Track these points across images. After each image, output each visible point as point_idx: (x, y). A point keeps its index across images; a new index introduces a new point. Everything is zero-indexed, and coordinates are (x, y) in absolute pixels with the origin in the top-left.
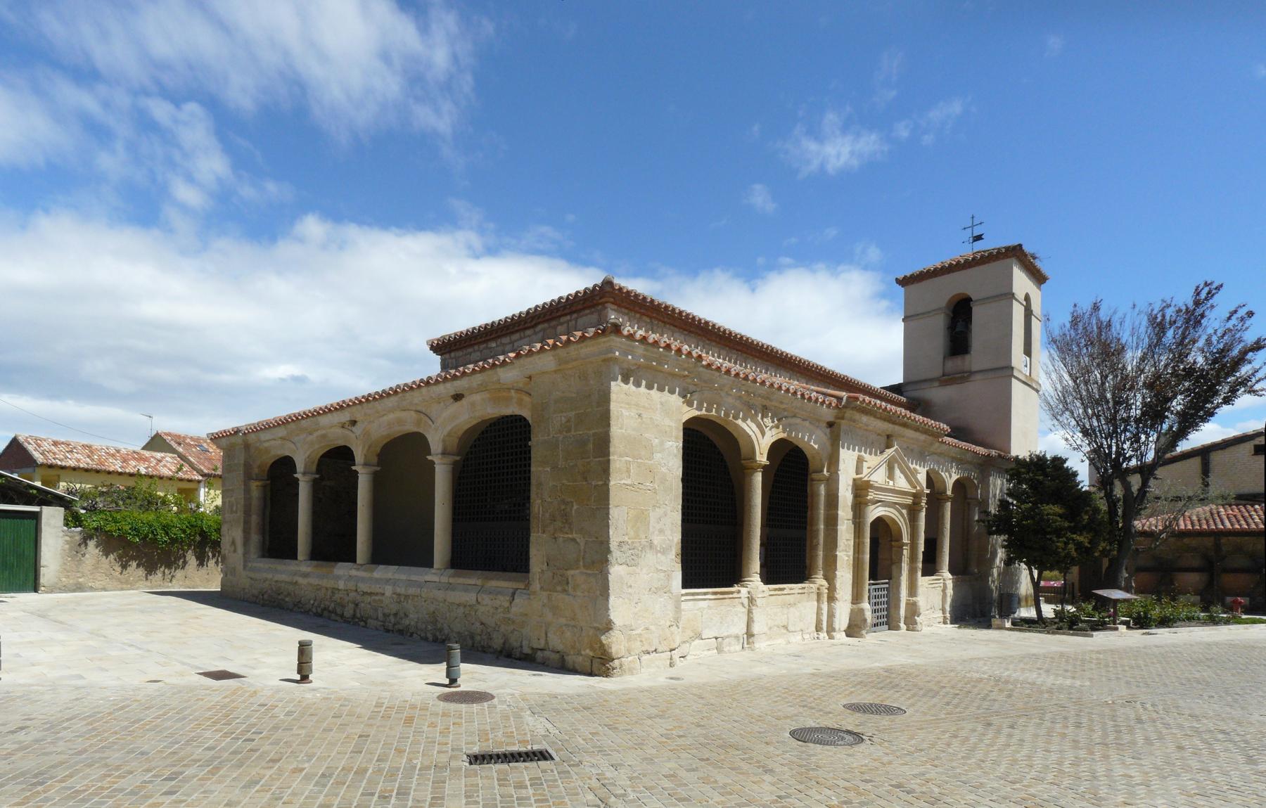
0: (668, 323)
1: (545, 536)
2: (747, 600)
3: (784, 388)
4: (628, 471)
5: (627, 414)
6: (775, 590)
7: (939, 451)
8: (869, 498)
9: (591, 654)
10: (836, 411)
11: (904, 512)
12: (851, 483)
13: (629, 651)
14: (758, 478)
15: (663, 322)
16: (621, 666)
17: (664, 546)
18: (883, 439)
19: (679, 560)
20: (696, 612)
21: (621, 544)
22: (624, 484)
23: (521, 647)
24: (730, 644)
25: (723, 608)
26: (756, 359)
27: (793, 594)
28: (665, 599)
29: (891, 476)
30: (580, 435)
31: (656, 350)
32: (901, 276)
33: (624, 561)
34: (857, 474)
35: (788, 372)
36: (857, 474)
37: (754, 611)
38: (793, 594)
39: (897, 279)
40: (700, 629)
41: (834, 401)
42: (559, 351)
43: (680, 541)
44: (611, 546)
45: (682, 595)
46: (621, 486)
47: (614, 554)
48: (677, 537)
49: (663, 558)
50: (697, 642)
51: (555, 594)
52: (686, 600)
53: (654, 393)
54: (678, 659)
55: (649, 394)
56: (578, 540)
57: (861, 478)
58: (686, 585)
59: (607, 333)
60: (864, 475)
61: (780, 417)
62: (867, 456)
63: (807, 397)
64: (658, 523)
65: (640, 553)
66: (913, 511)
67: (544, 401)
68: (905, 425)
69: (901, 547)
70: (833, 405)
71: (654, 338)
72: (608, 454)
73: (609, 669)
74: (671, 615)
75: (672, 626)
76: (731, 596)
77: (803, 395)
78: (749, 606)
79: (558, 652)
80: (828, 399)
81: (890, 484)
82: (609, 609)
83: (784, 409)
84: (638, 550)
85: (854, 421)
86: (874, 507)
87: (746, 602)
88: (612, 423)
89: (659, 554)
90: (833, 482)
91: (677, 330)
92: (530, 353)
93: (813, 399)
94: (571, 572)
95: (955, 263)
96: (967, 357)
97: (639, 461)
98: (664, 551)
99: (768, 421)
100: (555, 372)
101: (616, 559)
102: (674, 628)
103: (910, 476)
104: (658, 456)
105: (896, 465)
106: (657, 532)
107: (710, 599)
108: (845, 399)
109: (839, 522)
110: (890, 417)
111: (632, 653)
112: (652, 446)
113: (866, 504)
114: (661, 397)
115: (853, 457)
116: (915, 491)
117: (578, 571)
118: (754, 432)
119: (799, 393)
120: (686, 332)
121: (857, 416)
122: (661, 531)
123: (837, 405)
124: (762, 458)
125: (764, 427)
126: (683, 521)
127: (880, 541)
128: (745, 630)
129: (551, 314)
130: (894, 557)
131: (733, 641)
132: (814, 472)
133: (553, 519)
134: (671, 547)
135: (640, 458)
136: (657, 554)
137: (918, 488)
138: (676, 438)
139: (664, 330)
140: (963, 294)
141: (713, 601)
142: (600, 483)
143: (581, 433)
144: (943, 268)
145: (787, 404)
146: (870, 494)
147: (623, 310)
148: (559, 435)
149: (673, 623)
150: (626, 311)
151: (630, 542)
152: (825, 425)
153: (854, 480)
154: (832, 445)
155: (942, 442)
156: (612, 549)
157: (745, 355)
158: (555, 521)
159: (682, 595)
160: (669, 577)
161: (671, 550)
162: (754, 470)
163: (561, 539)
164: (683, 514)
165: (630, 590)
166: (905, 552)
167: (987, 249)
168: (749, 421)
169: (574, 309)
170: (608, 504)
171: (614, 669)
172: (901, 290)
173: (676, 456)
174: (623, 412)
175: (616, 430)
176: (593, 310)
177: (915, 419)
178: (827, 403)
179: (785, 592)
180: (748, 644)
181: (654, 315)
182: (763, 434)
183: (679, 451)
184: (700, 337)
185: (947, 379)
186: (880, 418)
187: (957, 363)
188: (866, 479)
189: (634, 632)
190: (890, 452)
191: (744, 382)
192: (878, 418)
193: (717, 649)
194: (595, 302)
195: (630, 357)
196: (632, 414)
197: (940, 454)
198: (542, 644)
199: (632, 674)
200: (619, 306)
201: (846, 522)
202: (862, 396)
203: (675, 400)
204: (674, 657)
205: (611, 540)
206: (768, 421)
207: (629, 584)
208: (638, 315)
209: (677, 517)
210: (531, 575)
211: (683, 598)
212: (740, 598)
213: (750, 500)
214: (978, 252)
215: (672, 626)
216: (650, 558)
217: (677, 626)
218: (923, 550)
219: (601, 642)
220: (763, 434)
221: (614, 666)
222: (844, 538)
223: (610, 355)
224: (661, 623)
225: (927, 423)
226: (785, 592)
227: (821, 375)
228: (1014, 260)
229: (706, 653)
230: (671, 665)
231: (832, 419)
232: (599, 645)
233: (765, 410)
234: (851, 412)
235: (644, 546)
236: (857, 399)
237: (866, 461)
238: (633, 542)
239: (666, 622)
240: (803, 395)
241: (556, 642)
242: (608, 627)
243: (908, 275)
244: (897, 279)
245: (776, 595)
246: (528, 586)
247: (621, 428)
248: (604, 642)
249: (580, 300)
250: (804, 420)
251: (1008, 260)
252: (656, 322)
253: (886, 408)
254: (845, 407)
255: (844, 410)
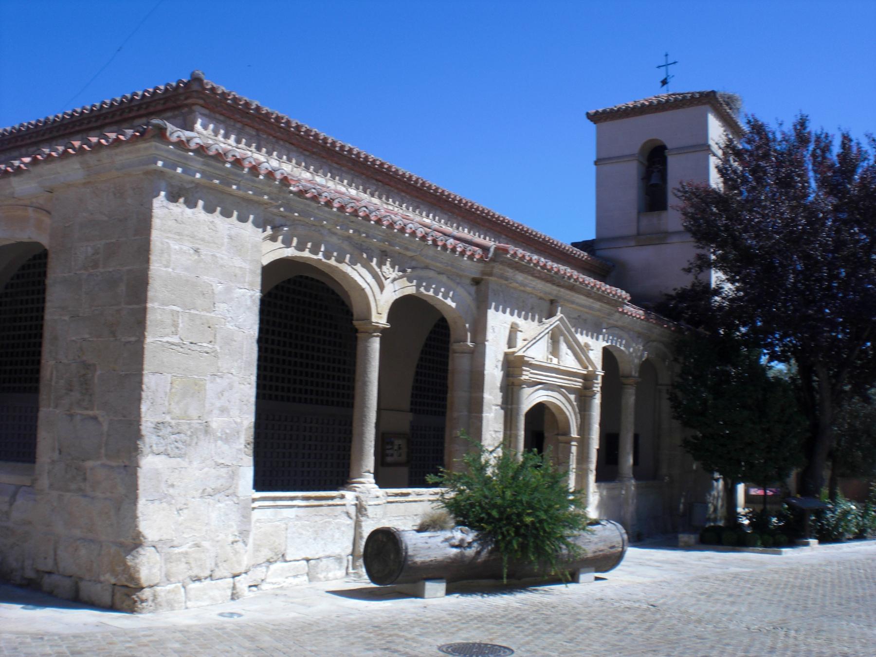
0: (282, 140)
1: (58, 411)
2: (354, 508)
3: (408, 231)
4: (175, 325)
5: (177, 247)
6: (396, 495)
7: (620, 323)
8: (523, 377)
9: (113, 581)
10: (481, 265)
11: (572, 397)
12: (501, 357)
13: (168, 578)
14: (375, 345)
15: (274, 137)
16: (155, 597)
17: (228, 431)
18: (546, 305)
19: (250, 450)
20: (278, 523)
21: (158, 426)
22: (168, 342)
23: (23, 568)
24: (328, 570)
25: (317, 519)
26: (403, 194)
27: (421, 501)
28: (227, 505)
29: (555, 351)
30: (110, 272)
31: (220, 165)
32: (592, 111)
33: (162, 449)
34: (509, 348)
35: (446, 214)
36: (509, 348)
37: (363, 524)
38: (421, 501)
39: (588, 114)
40: (283, 548)
41: (479, 251)
42: (87, 157)
43: (252, 425)
44: (143, 428)
45: (254, 500)
46: (163, 346)
47: (147, 440)
48: (247, 419)
49: (225, 447)
50: (278, 566)
51: (68, 495)
52: (260, 507)
53: (217, 218)
54: (246, 589)
55: (212, 222)
56: (101, 419)
57: (514, 353)
58: (262, 482)
59: (147, 136)
60: (519, 349)
61: (403, 263)
62: (521, 322)
63: (440, 243)
64: (219, 398)
65: (188, 439)
66: (583, 398)
67: (67, 225)
68: (572, 288)
69: (568, 443)
70: (477, 256)
71: (217, 150)
72: (144, 300)
73: (135, 602)
74: (235, 527)
75: (236, 542)
76: (330, 502)
77: (435, 241)
78: (357, 516)
79: (71, 577)
80: (470, 249)
81: (553, 362)
82: (137, 517)
83: (411, 257)
84: (186, 434)
85: (507, 279)
86: (532, 389)
87: (353, 511)
88: (153, 258)
89: (220, 443)
90: (478, 354)
91: (295, 149)
92: (49, 158)
93: (449, 247)
94: (90, 464)
95: (647, 103)
96: (664, 214)
97: (192, 311)
98: (227, 439)
99: (387, 269)
100: (84, 184)
101: (151, 447)
102: (240, 544)
103: (580, 353)
104: (222, 307)
105: (562, 338)
106: (216, 412)
107: (299, 507)
108: (492, 250)
109: (485, 408)
110: (552, 276)
111: (172, 580)
112: (213, 293)
113: (521, 385)
114: (229, 229)
115: (505, 325)
116: (585, 372)
117: (99, 462)
118: (368, 284)
119: (429, 238)
120: (307, 153)
121: (509, 272)
122: (223, 410)
123: (482, 257)
124: (380, 318)
125: (383, 279)
126: (258, 396)
127: (546, 434)
128: (350, 550)
129: (121, 115)
130: (561, 455)
131: (332, 564)
132: (455, 342)
133: (70, 389)
134: (238, 433)
135: (194, 308)
136: (216, 441)
137: (590, 369)
138: (251, 284)
139: (277, 146)
140: (660, 140)
141: (271, 510)
142: (133, 339)
143: (111, 270)
144: (635, 107)
145: (415, 251)
146: (524, 373)
147: (218, 116)
148: (83, 272)
149: (237, 539)
150: (222, 118)
151: (173, 422)
152: (468, 281)
153: (506, 354)
154: (478, 308)
155: (623, 313)
156: (144, 432)
157: (387, 187)
158: (71, 390)
159: (254, 500)
160: (233, 475)
161: (238, 438)
162: (369, 334)
163: (78, 418)
164: (258, 386)
165: (171, 491)
166: (574, 449)
167: (682, 92)
168: (358, 267)
169: (151, 109)
170: (142, 369)
171: (142, 601)
172: (592, 127)
173: (249, 308)
174: (172, 245)
175: (157, 268)
176: (176, 113)
177: (584, 281)
178: (468, 253)
179: (410, 498)
180: (353, 569)
181: (262, 127)
182: (382, 287)
183: (253, 301)
184: (324, 160)
185: (643, 239)
186: (539, 278)
187: (652, 221)
188: (520, 353)
189: (176, 550)
190: (554, 321)
191: (353, 219)
192: (536, 277)
193: (308, 574)
194: (179, 103)
195: (179, 170)
196: (185, 248)
197: (622, 328)
198: (49, 565)
199: (172, 608)
200: (212, 110)
201: (494, 408)
202: (513, 247)
203: (249, 232)
204: (238, 585)
205: (143, 419)
206: (387, 269)
207: (170, 482)
208: (239, 125)
209: (250, 391)
210: (37, 466)
211: (257, 504)
212: (344, 505)
213: (365, 372)
214: (673, 95)
215: (236, 542)
216: (206, 447)
217: (244, 542)
218: (597, 447)
219: (125, 564)
220: (382, 287)
221: (144, 597)
222: (491, 429)
223: (153, 167)
224: (219, 538)
225: (600, 288)
226: (410, 498)
227: (490, 221)
228: (708, 107)
229: (291, 580)
230: (234, 597)
231: (477, 276)
232: (122, 568)
233: (383, 256)
234: (501, 267)
235: (197, 429)
236: (506, 251)
237: (521, 331)
238: (178, 424)
239: (227, 535)
240: (435, 241)
241: (68, 562)
242: (136, 542)
243: (600, 110)
244: (588, 114)
245: (397, 502)
246: (34, 481)
247: (166, 267)
248: (129, 564)
249: (160, 99)
250: (439, 273)
251: (703, 107)
252: (265, 136)
253: (545, 265)
254: (493, 260)
255: (493, 264)
